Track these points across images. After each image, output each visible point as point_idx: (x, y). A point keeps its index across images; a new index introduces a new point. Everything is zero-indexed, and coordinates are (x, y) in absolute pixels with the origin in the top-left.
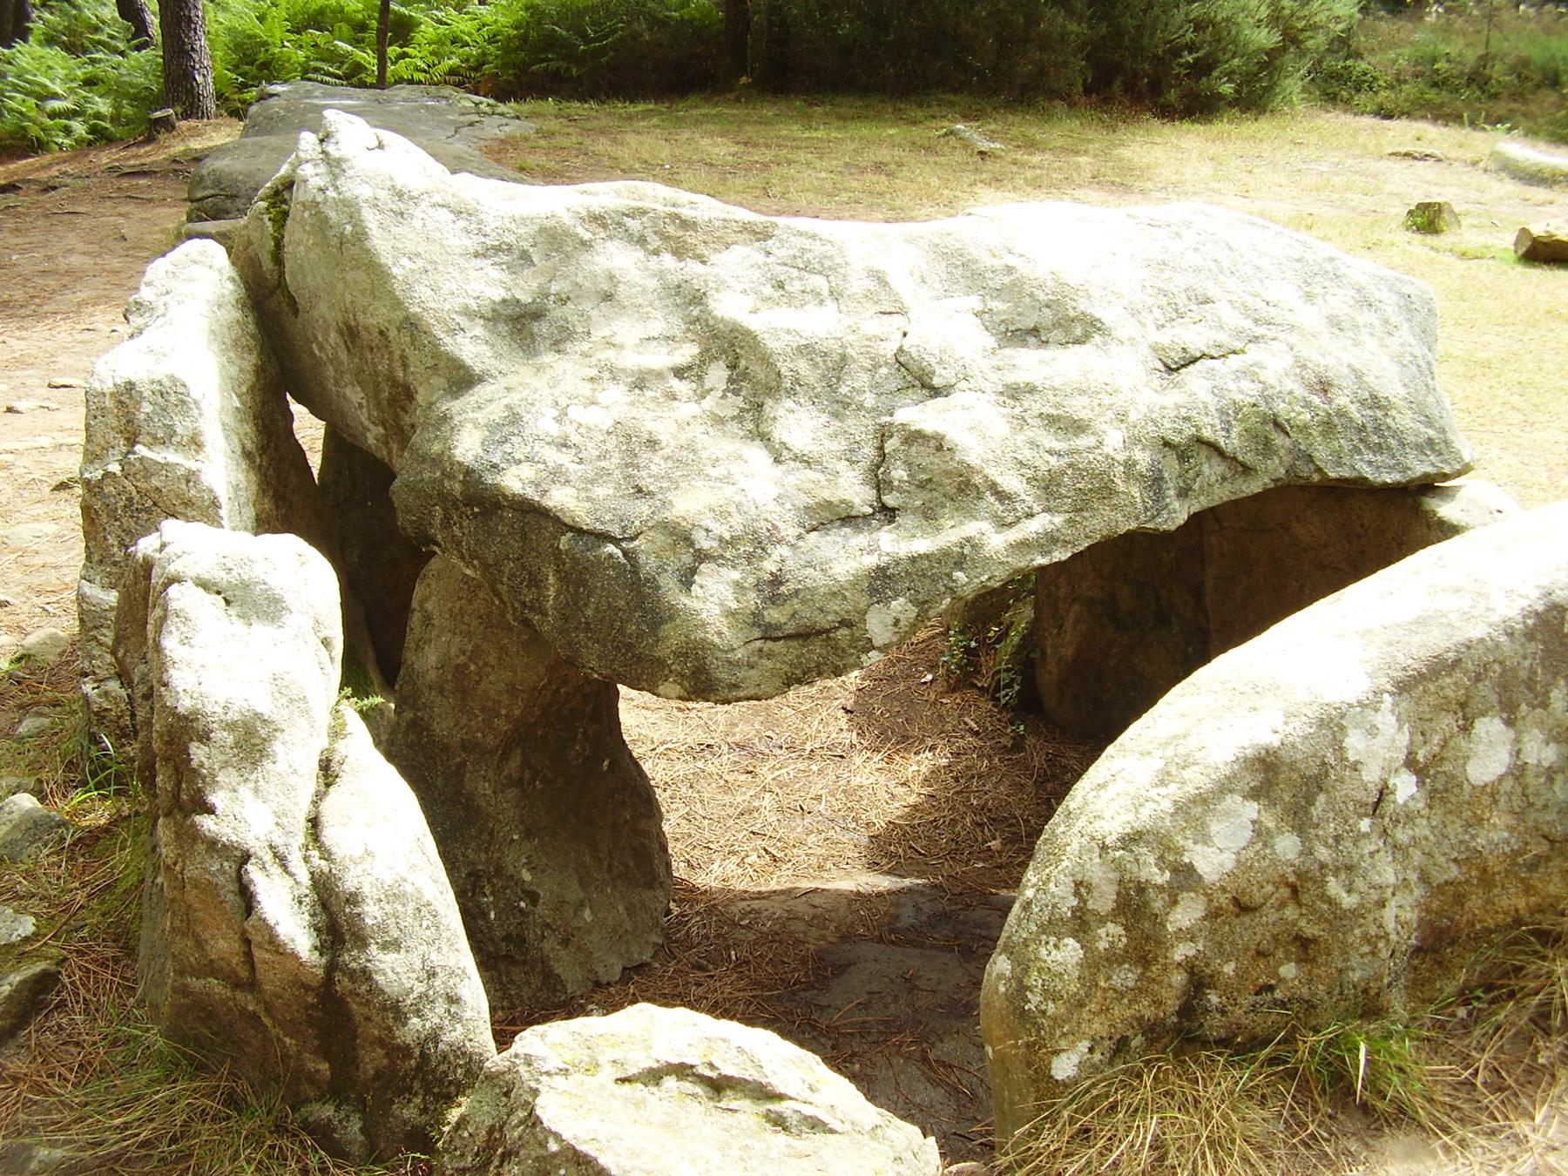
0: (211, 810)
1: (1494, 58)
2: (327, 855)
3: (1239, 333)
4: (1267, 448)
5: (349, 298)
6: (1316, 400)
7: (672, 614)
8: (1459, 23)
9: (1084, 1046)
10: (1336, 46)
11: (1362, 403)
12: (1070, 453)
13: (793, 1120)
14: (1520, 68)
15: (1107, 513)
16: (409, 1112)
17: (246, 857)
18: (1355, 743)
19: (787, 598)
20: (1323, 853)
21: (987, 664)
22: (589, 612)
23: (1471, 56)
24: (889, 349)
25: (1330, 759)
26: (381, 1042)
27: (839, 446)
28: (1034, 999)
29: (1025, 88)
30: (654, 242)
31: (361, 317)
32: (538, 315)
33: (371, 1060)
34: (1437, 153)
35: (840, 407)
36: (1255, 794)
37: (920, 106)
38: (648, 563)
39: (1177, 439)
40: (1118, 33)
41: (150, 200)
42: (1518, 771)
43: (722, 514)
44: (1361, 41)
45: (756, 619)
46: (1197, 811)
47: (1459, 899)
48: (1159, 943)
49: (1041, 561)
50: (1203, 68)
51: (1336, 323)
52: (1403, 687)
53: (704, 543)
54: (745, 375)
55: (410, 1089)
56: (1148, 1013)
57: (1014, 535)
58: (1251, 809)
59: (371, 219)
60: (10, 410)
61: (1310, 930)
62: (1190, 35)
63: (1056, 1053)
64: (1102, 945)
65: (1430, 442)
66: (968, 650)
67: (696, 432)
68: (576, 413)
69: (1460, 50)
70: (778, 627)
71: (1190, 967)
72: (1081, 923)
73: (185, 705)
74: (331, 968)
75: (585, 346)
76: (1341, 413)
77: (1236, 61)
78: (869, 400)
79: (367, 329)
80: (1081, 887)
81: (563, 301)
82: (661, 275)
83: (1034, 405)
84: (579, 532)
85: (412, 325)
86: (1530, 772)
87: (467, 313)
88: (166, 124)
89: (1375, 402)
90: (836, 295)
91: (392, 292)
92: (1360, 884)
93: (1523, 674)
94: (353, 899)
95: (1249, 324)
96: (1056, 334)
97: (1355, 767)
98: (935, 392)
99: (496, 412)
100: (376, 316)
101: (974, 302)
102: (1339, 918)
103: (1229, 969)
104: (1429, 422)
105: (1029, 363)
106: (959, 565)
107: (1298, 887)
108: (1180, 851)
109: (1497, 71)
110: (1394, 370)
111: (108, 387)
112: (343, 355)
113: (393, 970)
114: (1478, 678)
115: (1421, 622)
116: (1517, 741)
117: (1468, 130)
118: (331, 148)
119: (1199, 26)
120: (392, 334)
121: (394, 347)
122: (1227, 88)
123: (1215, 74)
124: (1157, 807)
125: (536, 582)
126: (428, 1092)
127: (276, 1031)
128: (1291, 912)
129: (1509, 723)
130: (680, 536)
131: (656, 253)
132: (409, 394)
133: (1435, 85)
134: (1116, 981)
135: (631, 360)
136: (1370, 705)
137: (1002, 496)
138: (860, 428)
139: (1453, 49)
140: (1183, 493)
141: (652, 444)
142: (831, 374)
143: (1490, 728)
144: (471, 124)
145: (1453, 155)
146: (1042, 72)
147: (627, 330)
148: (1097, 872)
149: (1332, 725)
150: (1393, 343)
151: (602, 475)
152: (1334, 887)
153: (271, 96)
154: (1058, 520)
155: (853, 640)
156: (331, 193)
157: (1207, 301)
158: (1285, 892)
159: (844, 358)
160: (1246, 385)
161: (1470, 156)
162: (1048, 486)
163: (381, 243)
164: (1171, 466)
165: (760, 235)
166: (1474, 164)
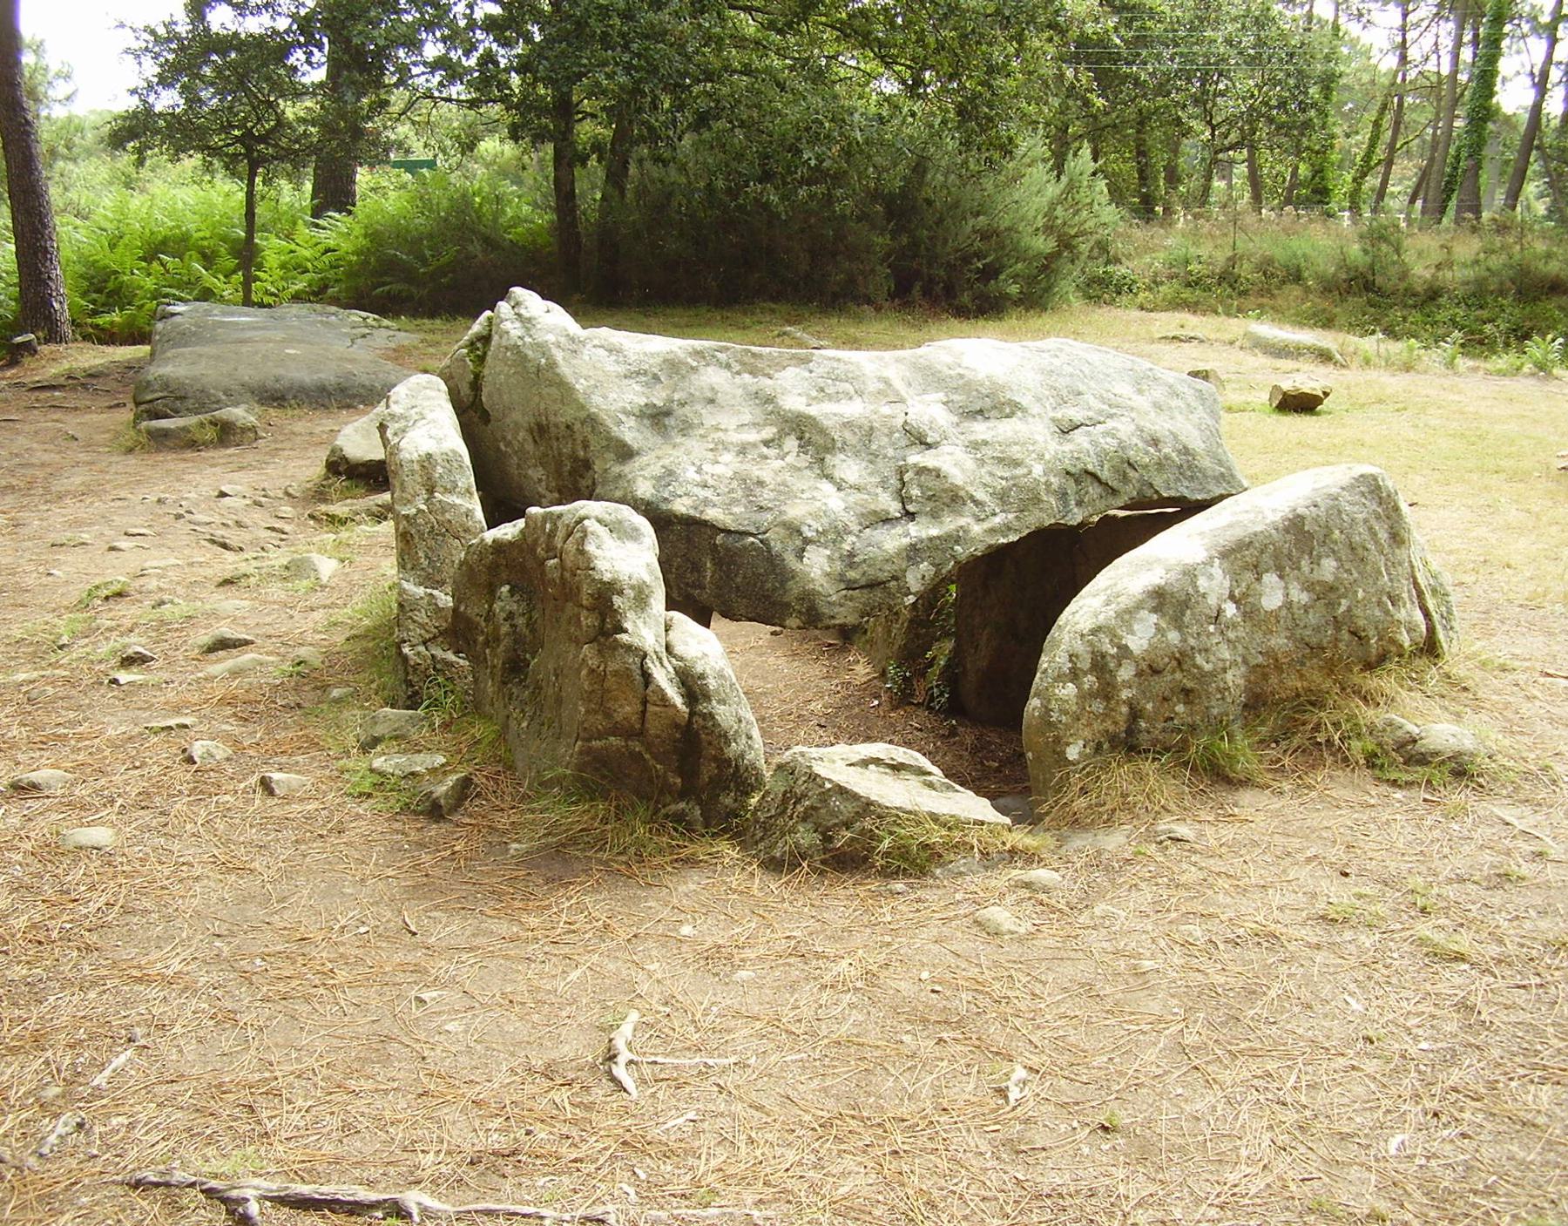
0: (626, 631)
1: (1241, 258)
2: (681, 659)
3: (1100, 412)
4: (1125, 478)
5: (542, 406)
6: (1152, 450)
7: (793, 575)
8: (1206, 227)
9: (1081, 743)
10: (1096, 252)
11: (1179, 452)
12: (1013, 478)
13: (937, 785)
14: (1266, 267)
15: (1037, 513)
16: (728, 800)
17: (645, 656)
18: (1202, 583)
19: (859, 564)
20: (1192, 642)
21: (920, 688)
22: (739, 580)
23: (1221, 257)
24: (899, 422)
25: (1191, 591)
26: (715, 759)
27: (875, 479)
28: (1055, 716)
29: (835, 296)
30: (737, 367)
31: (552, 418)
32: (668, 414)
33: (708, 771)
34: (1200, 335)
35: (874, 457)
36: (1154, 610)
37: (745, 313)
38: (777, 547)
39: (1073, 470)
40: (915, 244)
41: (76, 409)
42: (1288, 605)
43: (816, 517)
44: (1118, 247)
45: (841, 578)
46: (1127, 617)
47: (1265, 677)
48: (1114, 687)
49: (1003, 540)
50: (990, 273)
51: (1158, 406)
52: (1225, 555)
53: (809, 534)
54: (809, 442)
55: (728, 788)
56: (1111, 728)
57: (986, 525)
58: (1154, 618)
59: (559, 356)
60: (112, 549)
61: (1189, 684)
62: (977, 244)
63: (1068, 744)
64: (1086, 687)
65: (1222, 474)
66: (905, 679)
67: (787, 476)
68: (707, 467)
69: (1210, 253)
70: (855, 581)
71: (1130, 703)
72: (1075, 675)
73: (607, 577)
74: (692, 714)
75: (702, 432)
76: (1167, 458)
77: (1019, 265)
78: (891, 452)
79: (556, 426)
80: (1072, 657)
81: (683, 405)
82: (744, 387)
83: (988, 452)
84: (728, 532)
85: (592, 421)
86: (1295, 606)
87: (627, 413)
88: (28, 348)
89: (1185, 451)
90: (860, 393)
91: (576, 400)
92: (1212, 658)
93: (1285, 551)
94: (702, 676)
95: (1106, 407)
96: (994, 413)
97: (1204, 596)
98: (929, 446)
99: (657, 470)
100: (567, 415)
101: (941, 396)
102: (1203, 676)
103: (1149, 706)
104: (1220, 463)
105: (980, 430)
106: (957, 542)
107: (1181, 660)
108: (1121, 638)
109: (1245, 270)
110: (1196, 433)
111: (415, 456)
112: (530, 447)
113: (724, 714)
114: (1262, 552)
115: (1230, 526)
116: (1286, 588)
117: (1223, 317)
118: (523, 311)
119: (985, 235)
120: (577, 426)
121: (577, 435)
122: (1014, 289)
123: (1002, 277)
124: (1107, 615)
125: (697, 568)
126: (738, 789)
127: (652, 762)
128: (1178, 675)
129: (1281, 577)
130: (794, 530)
131: (738, 373)
132: (587, 465)
133: (1189, 285)
134: (1094, 708)
135: (736, 437)
136: (1209, 563)
137: (976, 503)
138: (888, 469)
139: (1204, 251)
140: (1079, 503)
141: (761, 483)
142: (865, 438)
143: (1270, 578)
144: (364, 336)
145: (1213, 336)
146: (852, 280)
147: (728, 421)
148: (1079, 647)
149: (1190, 573)
150: (1194, 417)
151: (734, 501)
152: (1199, 660)
153: (173, 315)
154: (1011, 516)
155: (900, 588)
156: (528, 339)
157: (1080, 394)
158: (1174, 663)
159: (872, 428)
160: (1109, 440)
161: (1227, 337)
162: (1002, 497)
163: (565, 370)
164: (1071, 487)
165: (805, 361)
166: (1231, 343)
